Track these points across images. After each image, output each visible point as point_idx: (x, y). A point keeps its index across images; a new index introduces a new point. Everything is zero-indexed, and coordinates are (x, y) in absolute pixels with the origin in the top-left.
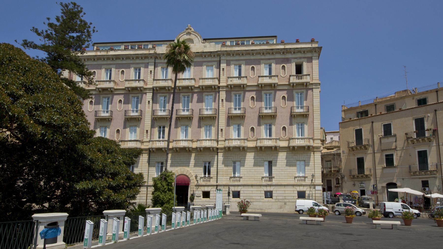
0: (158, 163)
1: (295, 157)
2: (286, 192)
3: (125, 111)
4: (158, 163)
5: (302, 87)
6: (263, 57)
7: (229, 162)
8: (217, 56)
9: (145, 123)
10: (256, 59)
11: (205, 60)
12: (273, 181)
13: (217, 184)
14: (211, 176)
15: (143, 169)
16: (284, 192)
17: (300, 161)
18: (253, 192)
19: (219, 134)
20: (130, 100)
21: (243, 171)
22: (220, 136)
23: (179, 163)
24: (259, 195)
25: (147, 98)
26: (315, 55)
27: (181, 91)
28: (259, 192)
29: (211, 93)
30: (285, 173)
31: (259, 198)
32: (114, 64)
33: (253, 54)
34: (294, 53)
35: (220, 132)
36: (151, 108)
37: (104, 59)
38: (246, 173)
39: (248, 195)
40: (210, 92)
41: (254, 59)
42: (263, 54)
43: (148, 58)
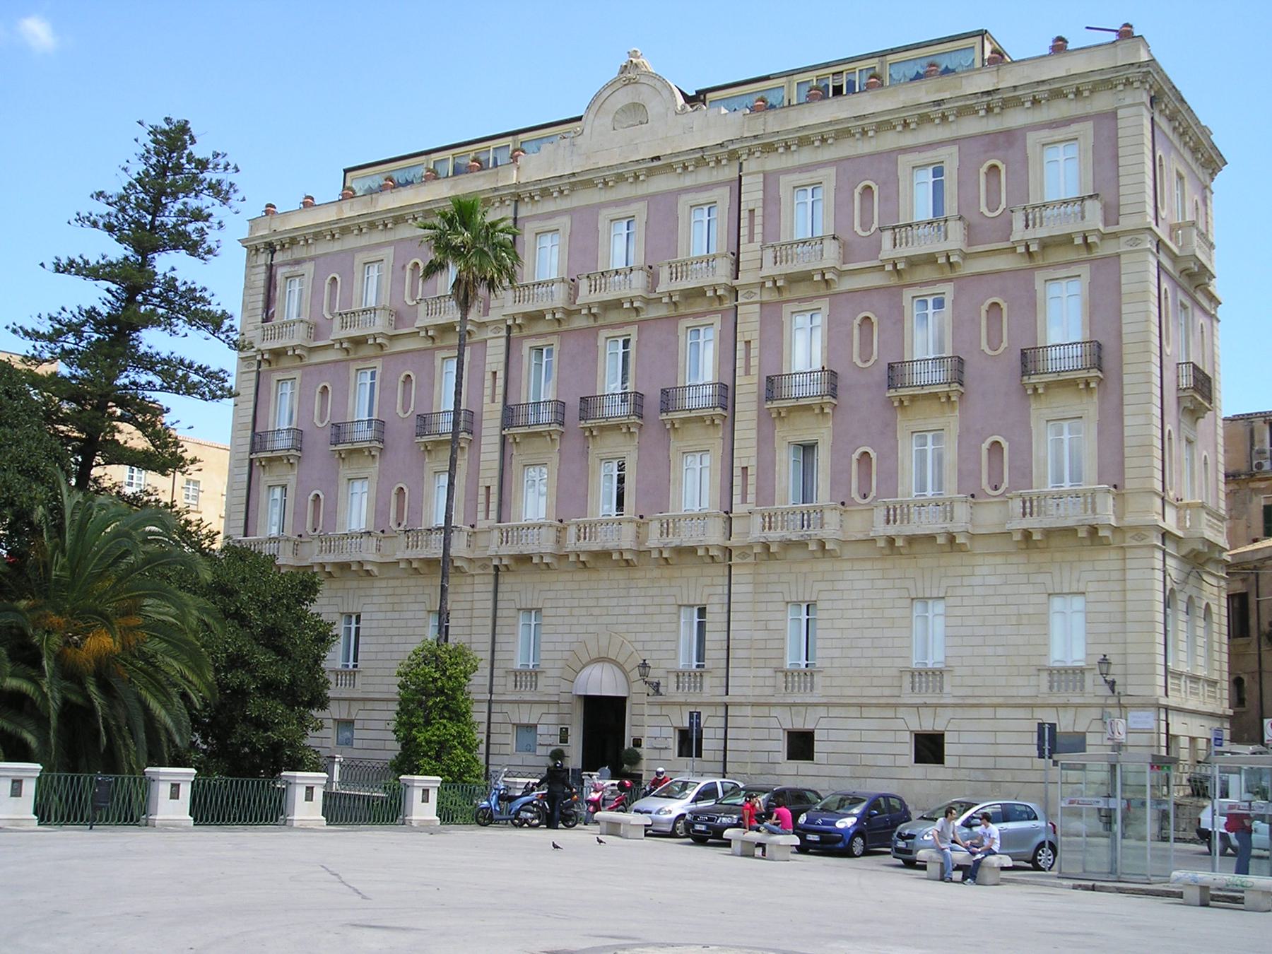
0: (798, 604)
1: (1040, 578)
2: (1001, 738)
3: (891, 367)
4: (798, 604)
5: (1072, 256)
6: (908, 140)
7: (771, 607)
8: (729, 160)
9: (482, 457)
10: (880, 153)
11: (688, 181)
12: (818, 691)
13: (726, 699)
14: (707, 664)
15: (474, 638)
16: (989, 738)
17: (924, 600)
18: (867, 736)
19: (737, 490)
20: (1039, 295)
21: (551, 647)
22: (737, 499)
23: (596, 611)
24: (888, 749)
25: (488, 359)
26: (1128, 101)
27: (682, 310)
28: (889, 736)
29: (1075, 270)
30: (1000, 651)
31: (887, 761)
32: (312, 259)
33: (944, 118)
34: (1036, 102)
35: (737, 481)
36: (499, 399)
37: (685, 168)
38: (837, 653)
39: (845, 747)
40: (704, 314)
41: (870, 155)
42: (1078, 93)
43: (933, 120)
